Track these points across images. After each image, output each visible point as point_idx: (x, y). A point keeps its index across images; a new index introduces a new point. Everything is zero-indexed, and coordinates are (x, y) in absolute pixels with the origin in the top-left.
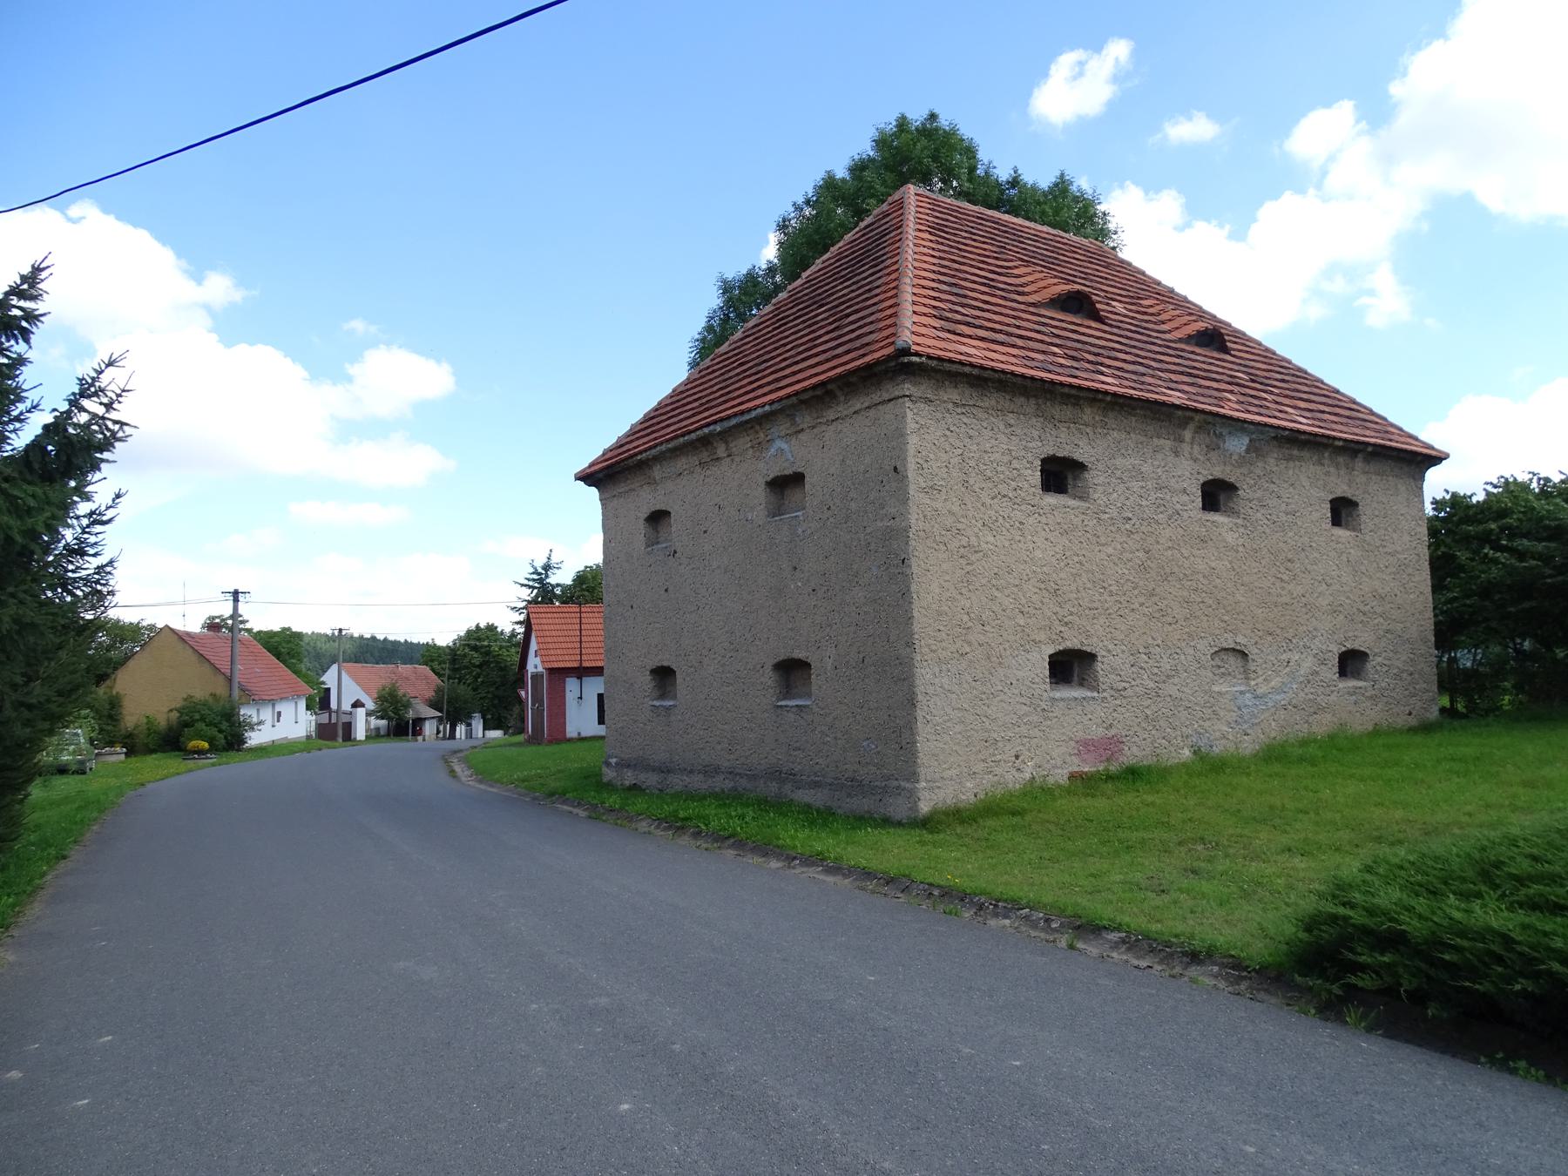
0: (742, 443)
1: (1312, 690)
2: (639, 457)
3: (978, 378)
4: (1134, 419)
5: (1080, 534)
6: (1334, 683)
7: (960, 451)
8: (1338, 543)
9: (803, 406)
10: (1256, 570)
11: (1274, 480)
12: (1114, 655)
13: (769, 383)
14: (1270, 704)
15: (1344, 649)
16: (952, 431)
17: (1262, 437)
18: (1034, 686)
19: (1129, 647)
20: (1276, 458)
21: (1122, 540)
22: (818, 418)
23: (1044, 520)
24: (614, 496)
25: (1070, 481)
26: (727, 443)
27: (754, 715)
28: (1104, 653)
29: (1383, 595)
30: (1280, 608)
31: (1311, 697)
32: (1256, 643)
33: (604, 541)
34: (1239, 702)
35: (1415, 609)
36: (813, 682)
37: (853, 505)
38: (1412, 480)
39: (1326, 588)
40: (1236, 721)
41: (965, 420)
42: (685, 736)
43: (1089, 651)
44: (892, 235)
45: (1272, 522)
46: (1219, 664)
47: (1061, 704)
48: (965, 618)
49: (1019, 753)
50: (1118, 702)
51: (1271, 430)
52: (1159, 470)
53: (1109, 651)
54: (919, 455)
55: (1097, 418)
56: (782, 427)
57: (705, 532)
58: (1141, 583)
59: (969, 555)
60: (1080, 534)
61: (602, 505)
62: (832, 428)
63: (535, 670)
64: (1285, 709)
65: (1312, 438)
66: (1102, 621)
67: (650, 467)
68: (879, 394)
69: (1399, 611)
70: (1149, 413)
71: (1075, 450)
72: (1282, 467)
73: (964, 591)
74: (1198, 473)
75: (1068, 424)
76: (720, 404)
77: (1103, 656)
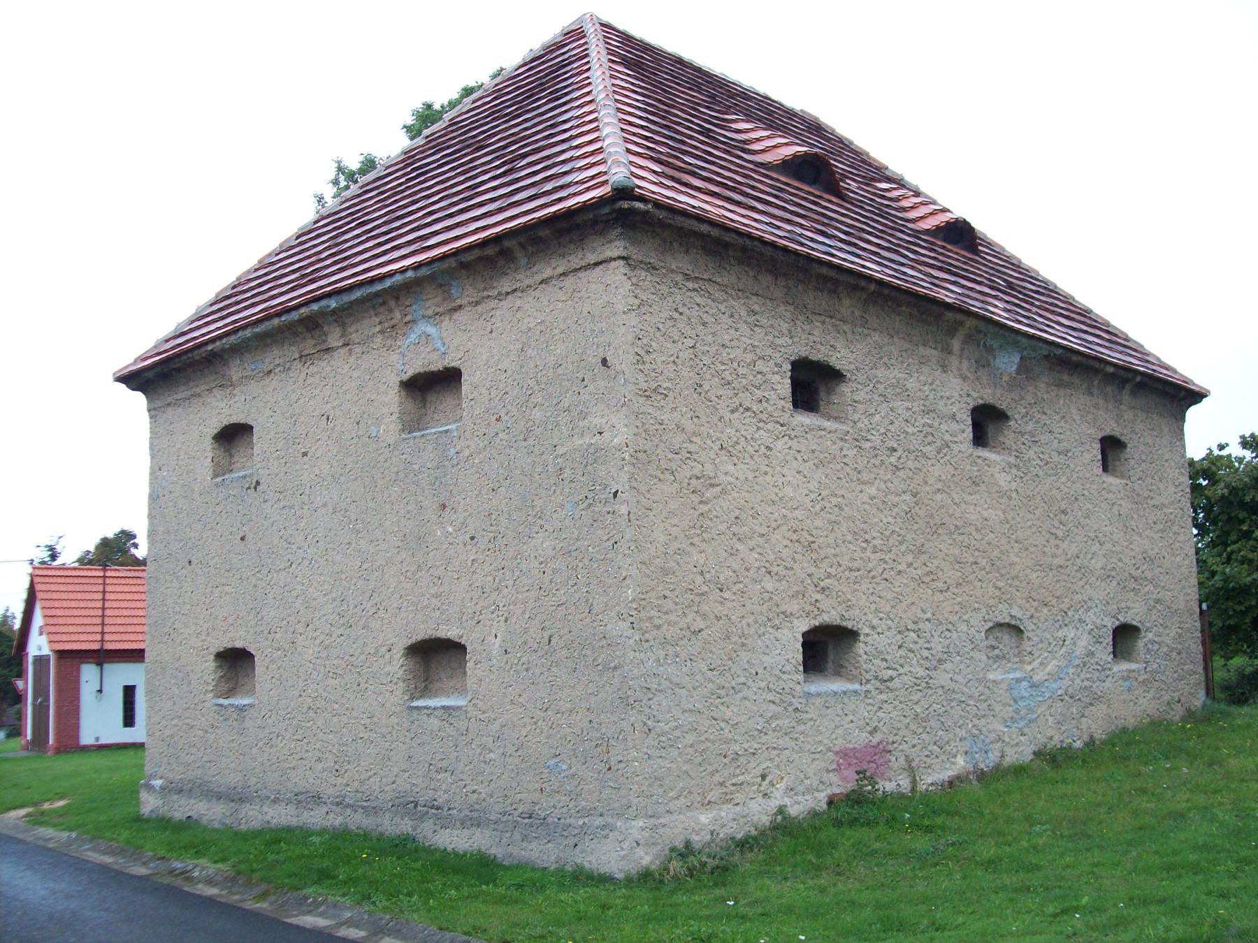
0: (369, 326)
1: (1088, 676)
2: (210, 347)
3: (718, 241)
4: (898, 318)
5: (838, 467)
6: (1109, 666)
7: (690, 342)
8: (1109, 492)
9: (464, 272)
10: (1029, 523)
11: (1046, 411)
12: (879, 633)
13: (409, 243)
14: (1047, 695)
15: (1117, 623)
16: (681, 314)
17: (1033, 355)
18: (785, 677)
19: (896, 622)
20: (1046, 383)
21: (886, 478)
22: (485, 289)
23: (794, 444)
24: (169, 405)
25: (823, 395)
26: (343, 325)
27: (375, 719)
28: (867, 630)
29: (1153, 557)
30: (1055, 572)
31: (1087, 683)
32: (1032, 617)
33: (151, 468)
34: (1015, 693)
35: (1182, 574)
36: (469, 672)
37: (537, 414)
38: (1174, 420)
39: (1100, 547)
40: (1012, 718)
41: (698, 300)
42: (267, 749)
43: (850, 627)
44: (575, 65)
45: (1044, 462)
46: (993, 643)
47: (818, 701)
48: (699, 579)
49: (766, 771)
50: (884, 697)
51: (1044, 346)
52: (926, 388)
53: (873, 628)
54: (639, 342)
55: (857, 313)
56: (430, 303)
57: (305, 454)
58: (908, 537)
59: (704, 490)
60: (838, 467)
61: (151, 417)
62: (505, 304)
63: (38, 653)
64: (1062, 700)
65: (1084, 361)
66: (864, 587)
67: (225, 363)
68: (580, 256)
69: (1167, 577)
70: (915, 312)
71: (830, 353)
72: (1053, 394)
73: (696, 540)
74: (968, 395)
75: (824, 317)
76: (333, 274)
77: (867, 635)
